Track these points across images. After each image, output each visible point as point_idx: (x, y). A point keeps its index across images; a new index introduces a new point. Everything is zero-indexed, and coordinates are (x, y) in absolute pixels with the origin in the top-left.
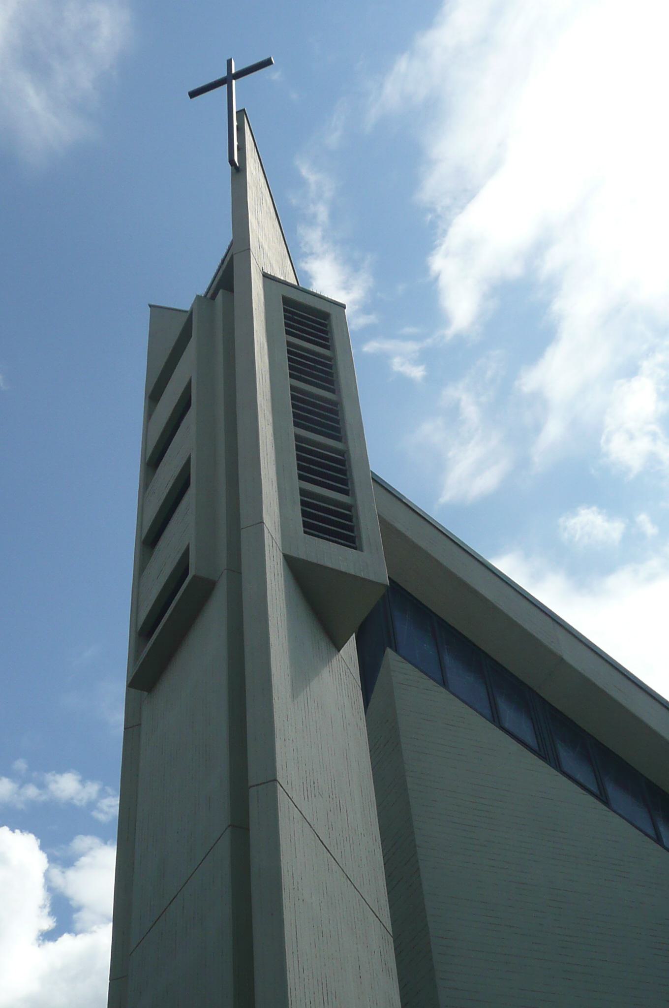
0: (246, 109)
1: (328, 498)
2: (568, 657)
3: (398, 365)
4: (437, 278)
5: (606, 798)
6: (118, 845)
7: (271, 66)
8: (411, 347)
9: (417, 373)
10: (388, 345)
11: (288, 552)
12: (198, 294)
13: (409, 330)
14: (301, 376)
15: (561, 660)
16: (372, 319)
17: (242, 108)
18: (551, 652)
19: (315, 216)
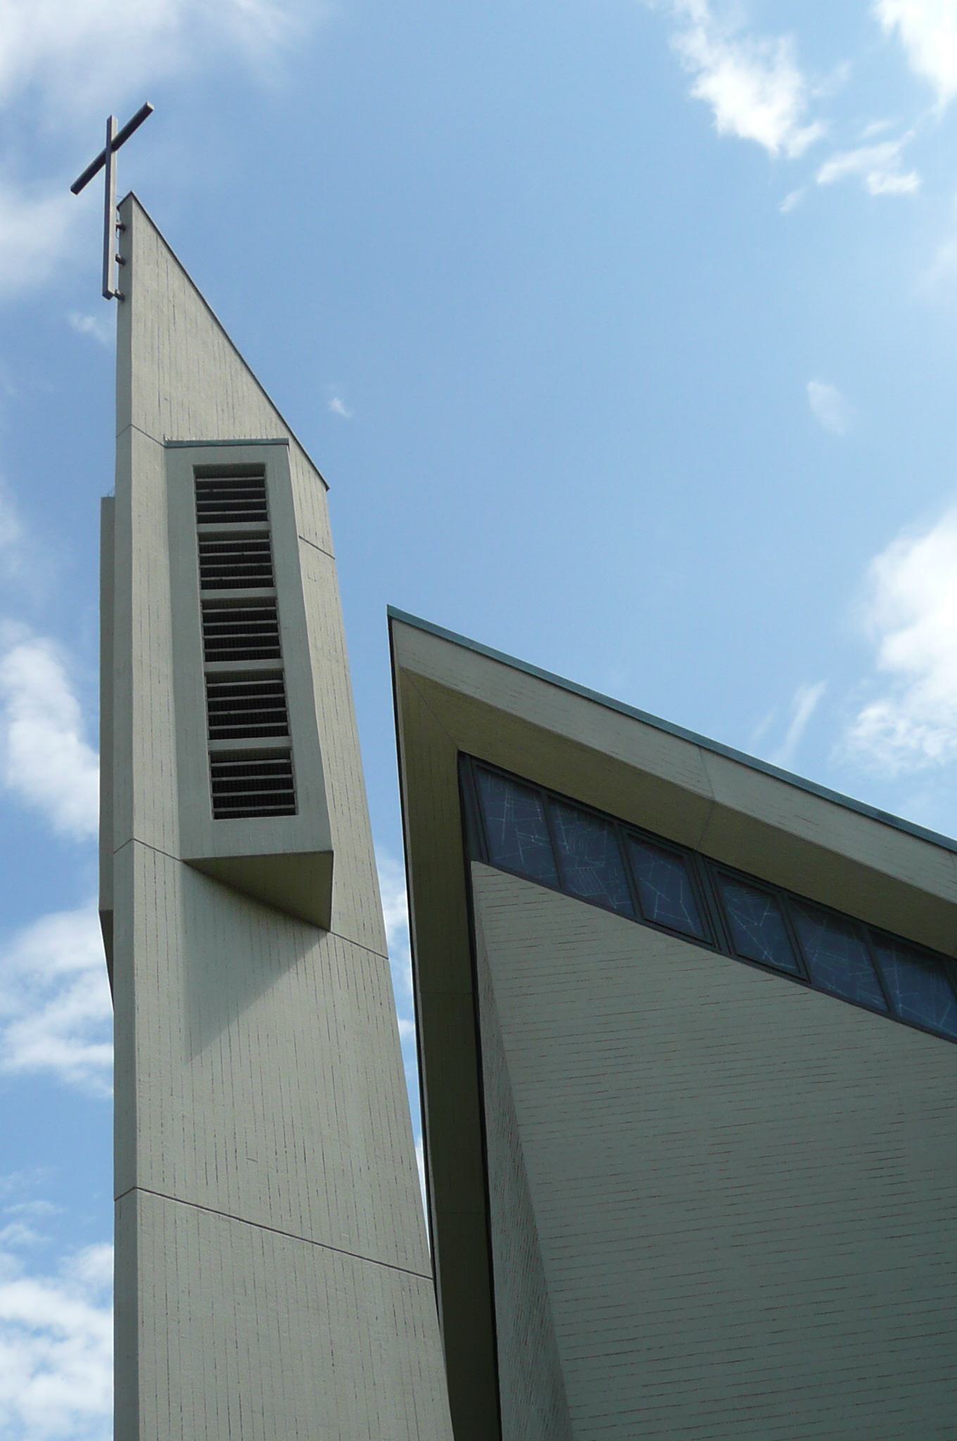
0: (134, 192)
1: (261, 751)
2: (724, 797)
3: (877, 184)
4: (897, 26)
5: (808, 974)
6: (115, 1246)
7: (152, 114)
8: (887, 151)
9: (909, 183)
10: (848, 162)
11: (189, 857)
12: (103, 496)
13: (874, 127)
14: (221, 580)
15: (713, 804)
16: (813, 133)
17: (128, 192)
18: (701, 798)
19: (687, 15)
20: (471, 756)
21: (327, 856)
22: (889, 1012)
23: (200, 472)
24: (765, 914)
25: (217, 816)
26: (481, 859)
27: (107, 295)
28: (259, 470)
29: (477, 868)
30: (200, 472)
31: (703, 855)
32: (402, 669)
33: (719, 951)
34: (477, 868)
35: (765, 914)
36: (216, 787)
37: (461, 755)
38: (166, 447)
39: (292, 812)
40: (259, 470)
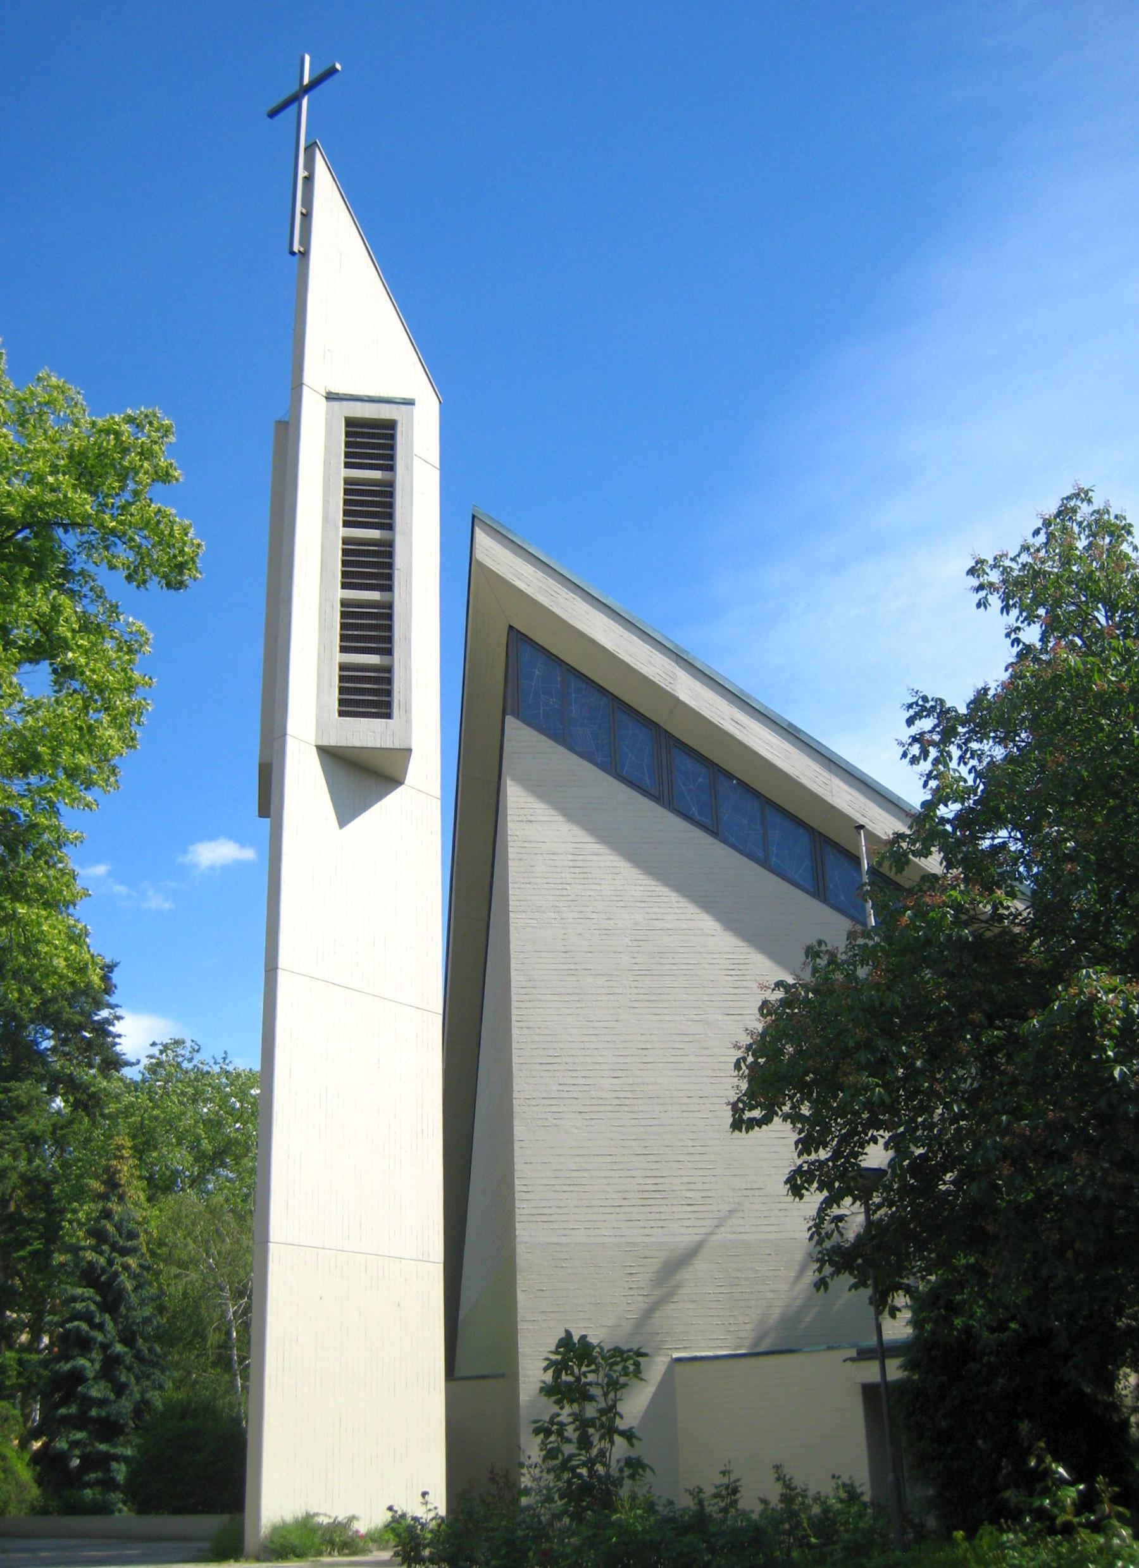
2: (684, 697)
11: (325, 743)
20: (518, 631)
21: (409, 751)
22: (765, 863)
23: (350, 423)
24: (700, 780)
25: (341, 651)
26: (513, 714)
27: (293, 253)
28: (390, 426)
29: (509, 720)
30: (350, 423)
31: (666, 731)
32: (479, 563)
33: (663, 805)
34: (509, 720)
35: (700, 780)
36: (342, 690)
37: (511, 627)
38: (326, 398)
39: (389, 716)
40: (390, 426)
